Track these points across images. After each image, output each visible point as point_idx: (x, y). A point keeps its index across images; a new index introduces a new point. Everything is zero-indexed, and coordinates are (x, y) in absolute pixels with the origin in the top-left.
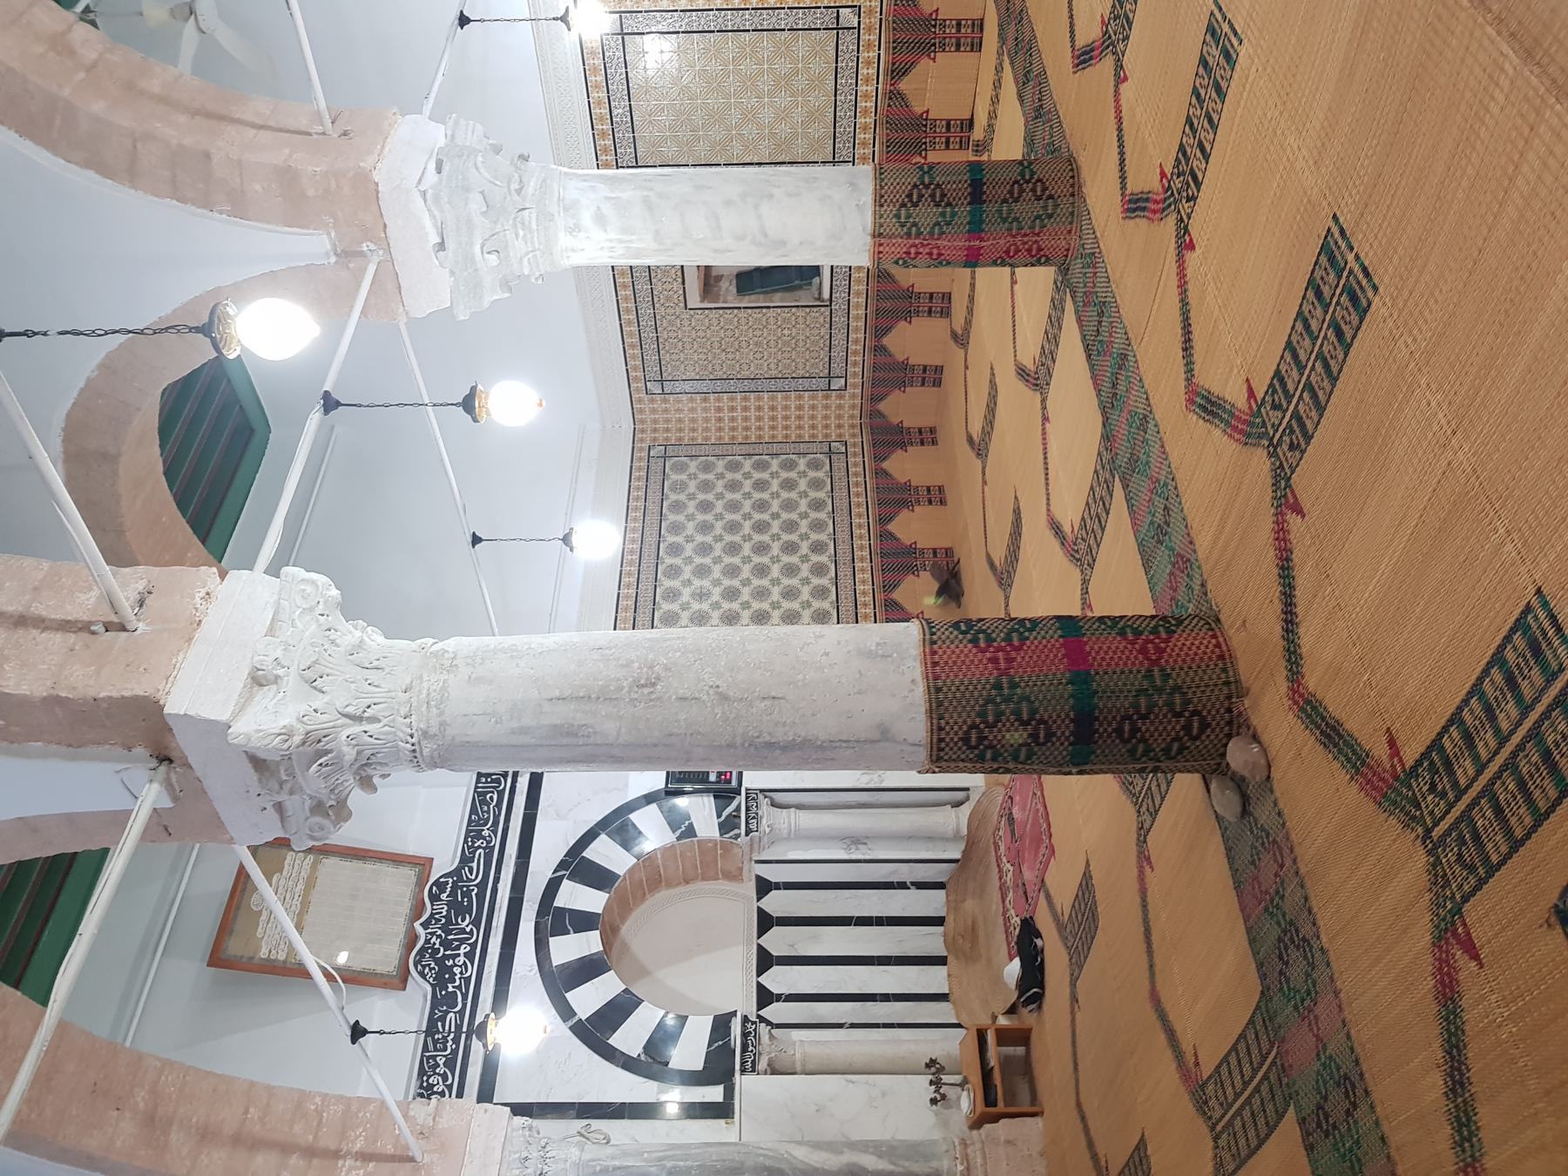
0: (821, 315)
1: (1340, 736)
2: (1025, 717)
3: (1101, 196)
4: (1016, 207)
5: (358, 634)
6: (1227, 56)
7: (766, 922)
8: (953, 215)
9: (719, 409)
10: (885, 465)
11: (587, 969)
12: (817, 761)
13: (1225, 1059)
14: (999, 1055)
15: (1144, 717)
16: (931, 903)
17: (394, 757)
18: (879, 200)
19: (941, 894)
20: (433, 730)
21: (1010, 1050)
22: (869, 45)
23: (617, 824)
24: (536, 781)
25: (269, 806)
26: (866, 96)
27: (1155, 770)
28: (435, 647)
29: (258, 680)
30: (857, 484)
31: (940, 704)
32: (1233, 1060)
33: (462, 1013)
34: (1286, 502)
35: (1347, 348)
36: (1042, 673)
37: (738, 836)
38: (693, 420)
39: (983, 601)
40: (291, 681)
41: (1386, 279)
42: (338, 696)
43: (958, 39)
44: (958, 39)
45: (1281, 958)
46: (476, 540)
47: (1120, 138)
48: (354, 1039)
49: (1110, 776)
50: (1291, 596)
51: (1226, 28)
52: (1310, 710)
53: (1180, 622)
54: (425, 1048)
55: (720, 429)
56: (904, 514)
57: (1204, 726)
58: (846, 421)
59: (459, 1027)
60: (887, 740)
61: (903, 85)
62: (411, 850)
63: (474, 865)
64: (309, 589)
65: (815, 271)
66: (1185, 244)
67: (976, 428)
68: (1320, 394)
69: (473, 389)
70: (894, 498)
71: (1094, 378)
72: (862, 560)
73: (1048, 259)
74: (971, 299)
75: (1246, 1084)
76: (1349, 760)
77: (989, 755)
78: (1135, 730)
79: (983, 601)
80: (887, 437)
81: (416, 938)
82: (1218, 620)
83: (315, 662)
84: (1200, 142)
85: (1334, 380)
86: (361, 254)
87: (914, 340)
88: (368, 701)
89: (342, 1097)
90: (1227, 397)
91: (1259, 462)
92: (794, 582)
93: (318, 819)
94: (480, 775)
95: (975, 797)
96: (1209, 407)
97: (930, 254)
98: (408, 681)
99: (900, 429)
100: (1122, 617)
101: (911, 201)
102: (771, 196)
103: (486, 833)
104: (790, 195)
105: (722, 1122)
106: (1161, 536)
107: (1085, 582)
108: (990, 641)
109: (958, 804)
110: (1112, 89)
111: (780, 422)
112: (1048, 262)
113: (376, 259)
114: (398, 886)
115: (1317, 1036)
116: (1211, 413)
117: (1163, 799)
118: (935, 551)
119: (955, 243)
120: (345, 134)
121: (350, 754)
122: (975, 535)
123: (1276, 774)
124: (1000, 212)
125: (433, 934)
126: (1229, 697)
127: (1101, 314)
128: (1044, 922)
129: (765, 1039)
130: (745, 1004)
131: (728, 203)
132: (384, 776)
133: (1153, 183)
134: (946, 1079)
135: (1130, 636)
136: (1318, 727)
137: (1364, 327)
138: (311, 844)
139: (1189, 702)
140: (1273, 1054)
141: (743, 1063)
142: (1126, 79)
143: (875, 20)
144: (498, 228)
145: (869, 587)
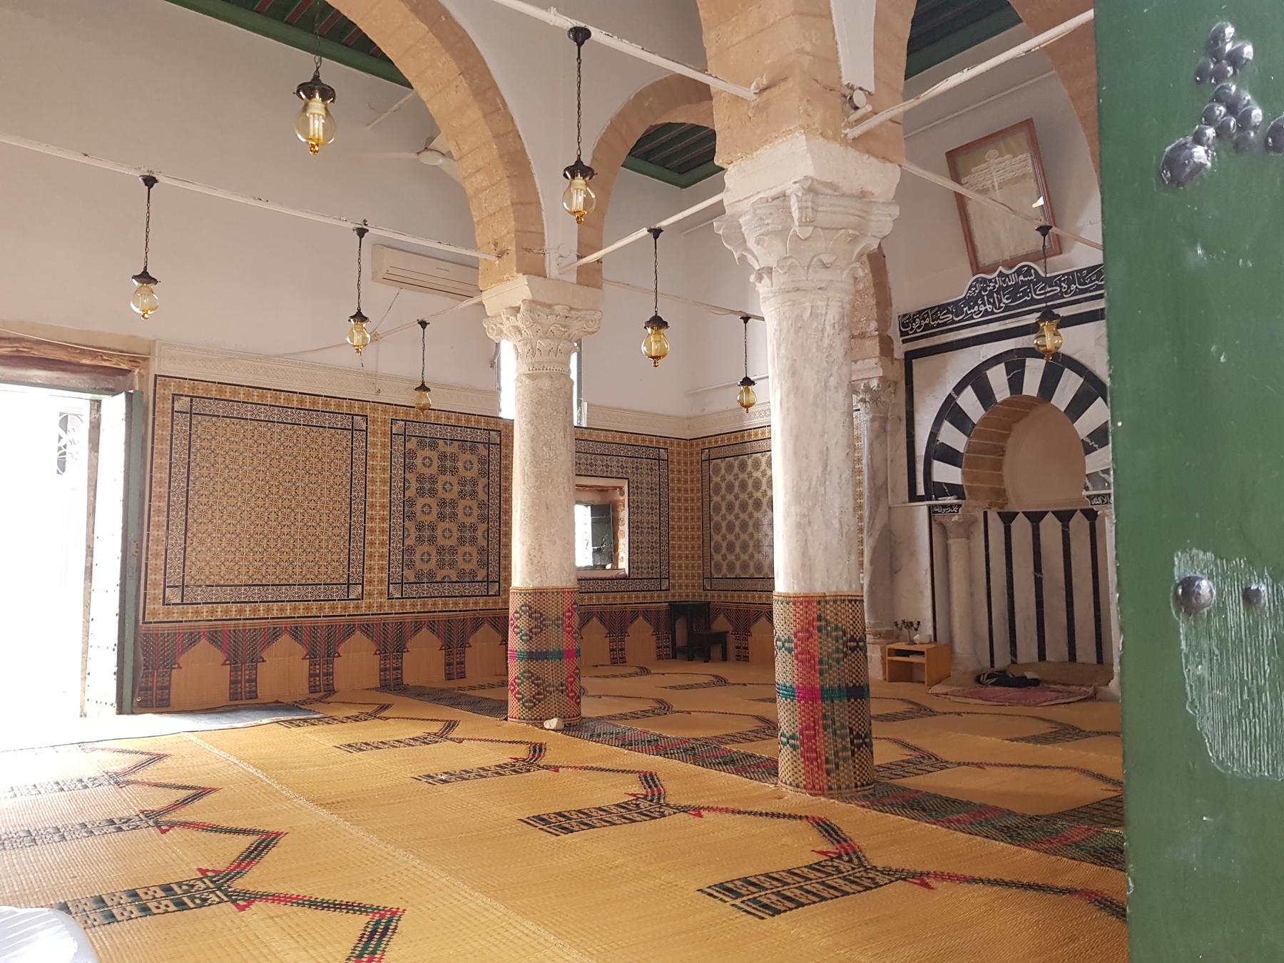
7: (1064, 517)
103: (1073, 287)
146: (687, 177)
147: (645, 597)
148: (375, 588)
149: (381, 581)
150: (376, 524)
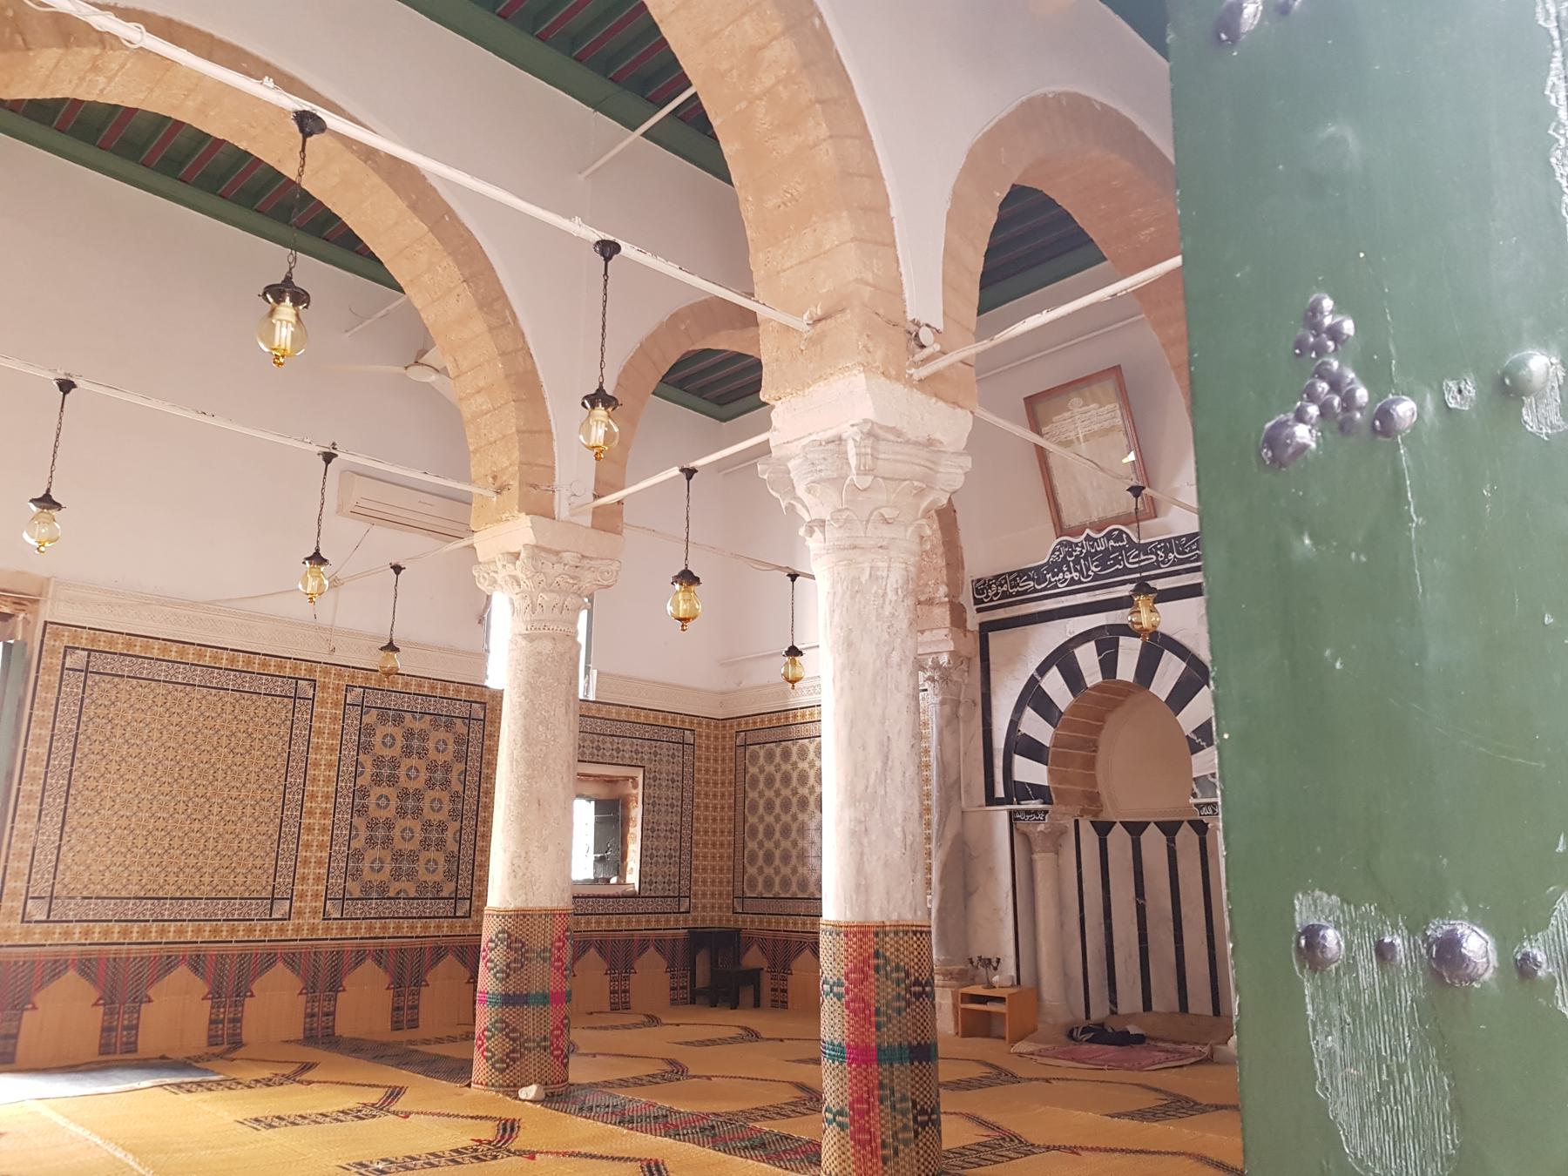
30: (384, 928)
99: (629, 968)
103: (1171, 556)
108: (557, 1037)
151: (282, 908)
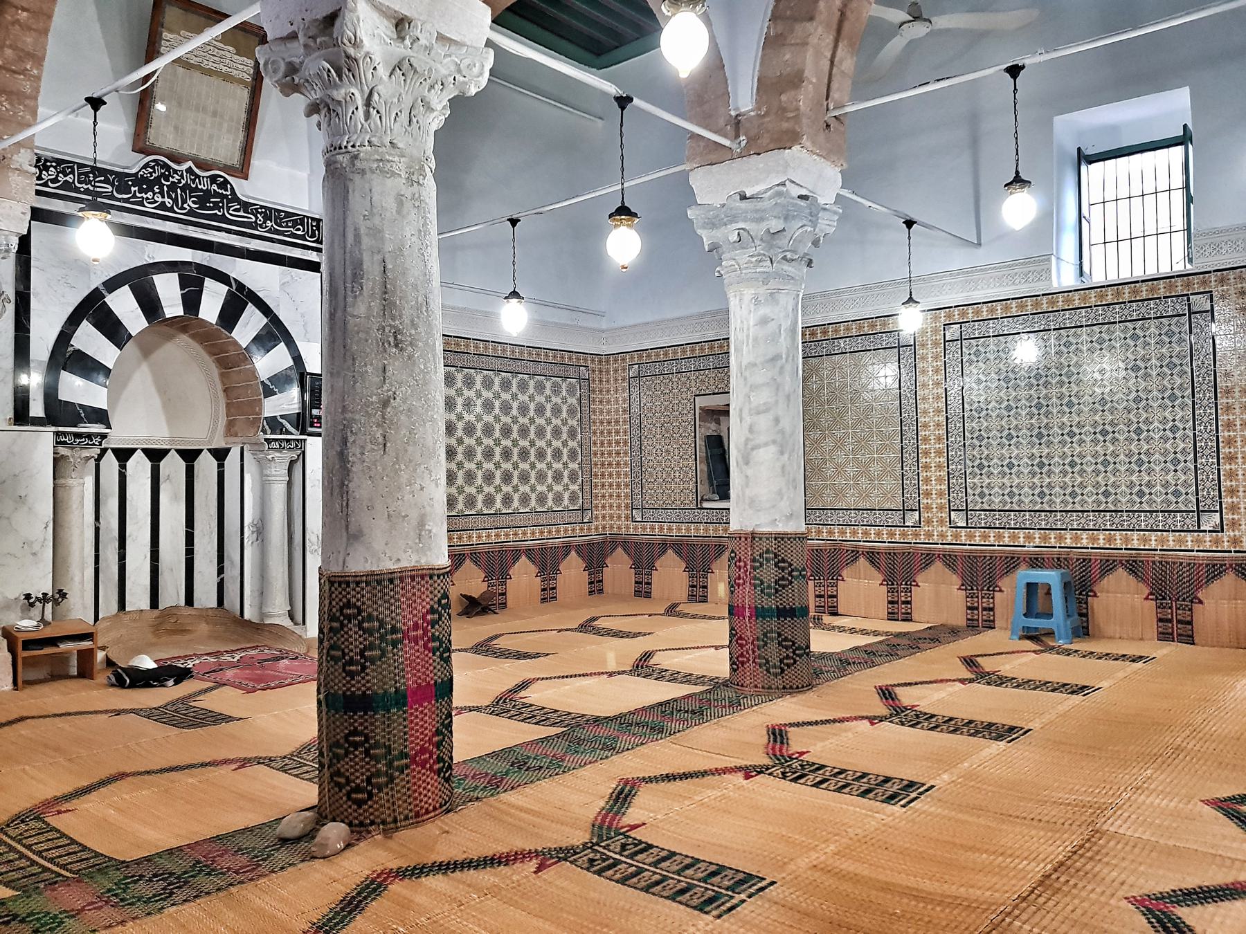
0: (690, 501)
1: (350, 913)
2: (368, 653)
3: (784, 709)
4: (775, 644)
5: (439, 107)
6: (892, 797)
7: (190, 456)
8: (769, 595)
9: (617, 432)
10: (573, 553)
11: (150, 304)
12: (333, 200)
13: (63, 835)
14: (69, 652)
15: (367, 752)
16: (206, 595)
17: (336, 132)
18: (780, 537)
19: (213, 603)
20: (358, 163)
21: (74, 662)
22: (892, 535)
23: (275, 332)
24: (314, 267)
25: (294, 28)
26: (854, 533)
27: (322, 765)
28: (428, 170)
29: (401, 24)
31: (379, 582)
32: (64, 841)
33: (112, 197)
34: (546, 858)
35: (672, 898)
36: (405, 667)
37: (265, 432)
38: (609, 402)
39: (464, 632)
40: (400, 50)
41: (726, 925)
42: (387, 87)
43: (897, 602)
44: (897, 602)
45: (155, 875)
46: (514, 222)
47: (828, 721)
48: (89, 100)
49: (314, 731)
50: (469, 867)
51: (913, 795)
52: (373, 888)
53: (447, 780)
54: (80, 166)
55: (602, 422)
56: (533, 569)
57: (359, 803)
58: (608, 522)
59: (99, 194)
60: (348, 539)
61: (862, 562)
62: (256, 163)
63: (241, 213)
64: (476, 70)
65: (725, 496)
66: (749, 772)
67: (602, 623)
68: (635, 880)
69: (635, 215)
70: (547, 561)
71: (644, 709)
72: (497, 535)
73: (735, 670)
74: (704, 617)
75: (39, 854)
76: (330, 920)
77: (336, 625)
78: (356, 745)
79: (464, 632)
80: (595, 555)
81: (179, 163)
82: (448, 811)
83: (416, 71)
84: (827, 780)
85: (646, 889)
86: (737, 136)
87: (671, 575)
88: (383, 112)
89: (38, 92)
90: (630, 810)
91: (579, 837)
92: (479, 481)
93: (283, 67)
94: (319, 221)
95: (298, 630)
96: (623, 795)
97: (739, 578)
98: (400, 145)
100: (451, 732)
101: (779, 562)
102: (782, 453)
103: (269, 224)
104: (783, 467)
105: (11, 415)
106: (517, 765)
107: (479, 709)
108: (433, 623)
109: (291, 616)
110: (864, 714)
111: (607, 471)
112: (733, 671)
113: (734, 146)
114: (225, 149)
115: (83, 909)
116: (618, 797)
117: (296, 776)
118: (504, 594)
119: (748, 596)
120: (828, 126)
121: (339, 95)
122: (518, 624)
123: (317, 864)
124: (771, 631)
125: (182, 176)
126: (384, 822)
127: (693, 712)
128: (187, 687)
129: (86, 453)
130: (118, 436)
131: (777, 420)
132: (319, 125)
133: (795, 746)
134: (49, 606)
135: (435, 739)
136: (359, 894)
137: (688, 909)
138: (262, 62)
139: (380, 790)
140: (68, 874)
141: (64, 434)
142: (872, 724)
143: (910, 539)
144: (757, 242)
145: (474, 540)
146: (604, 59)
147: (516, 534)
148: (935, 515)
149: (941, 508)
150: (933, 446)
151: (912, 518)
